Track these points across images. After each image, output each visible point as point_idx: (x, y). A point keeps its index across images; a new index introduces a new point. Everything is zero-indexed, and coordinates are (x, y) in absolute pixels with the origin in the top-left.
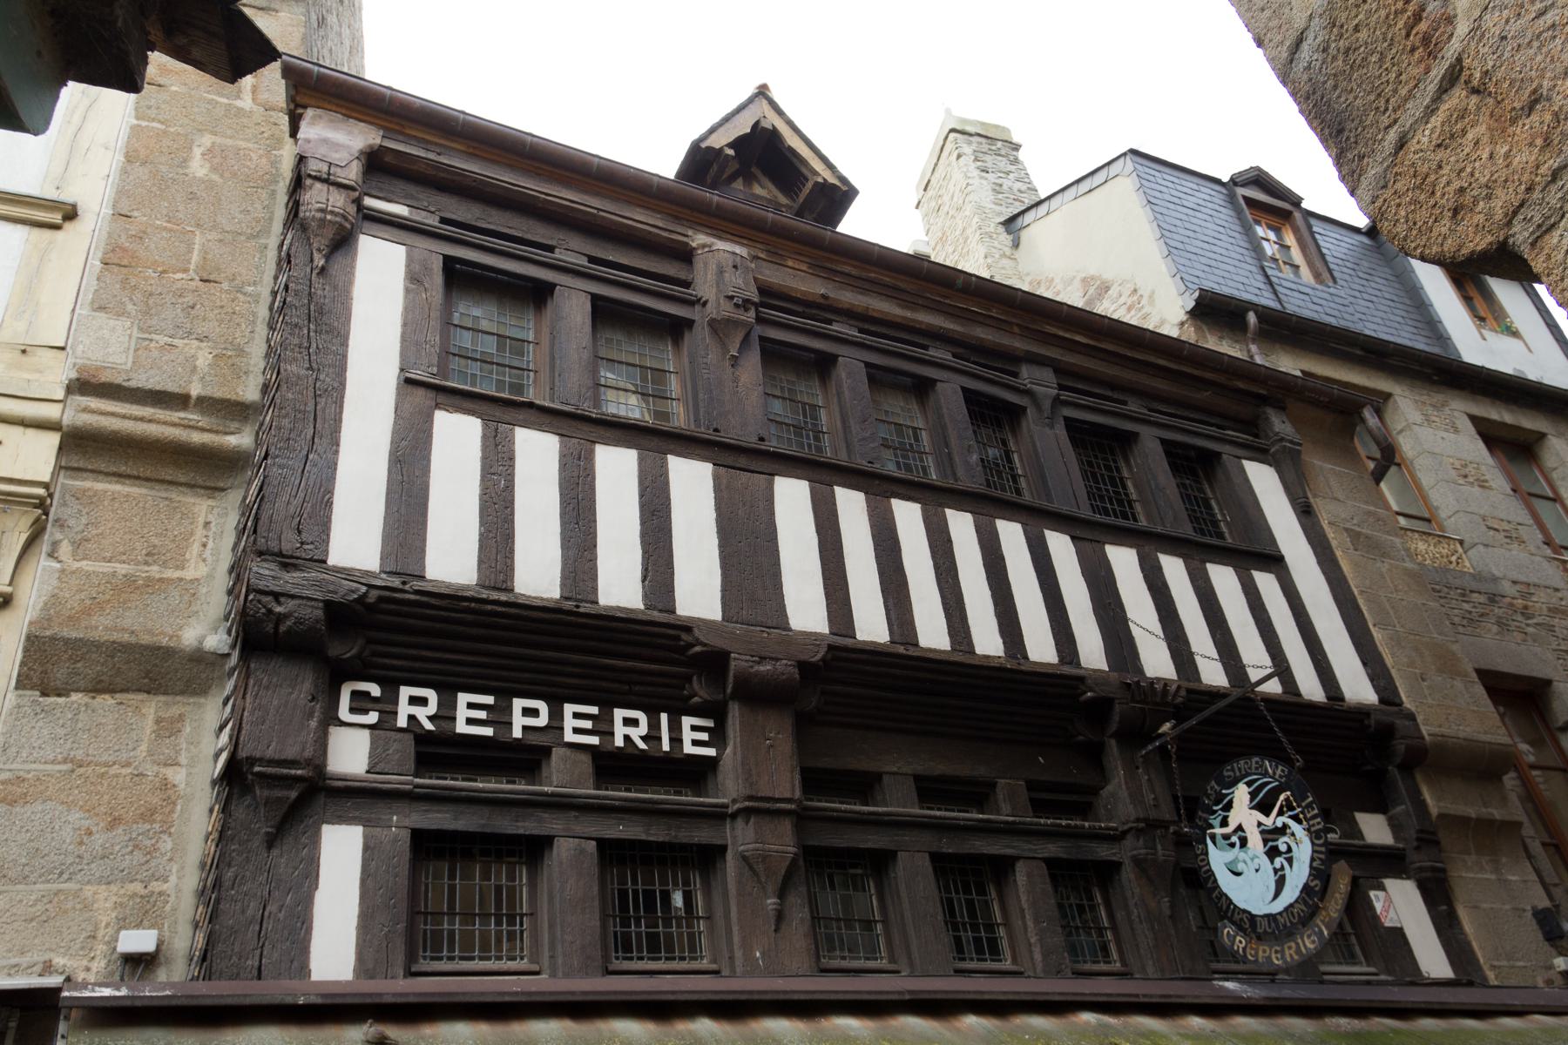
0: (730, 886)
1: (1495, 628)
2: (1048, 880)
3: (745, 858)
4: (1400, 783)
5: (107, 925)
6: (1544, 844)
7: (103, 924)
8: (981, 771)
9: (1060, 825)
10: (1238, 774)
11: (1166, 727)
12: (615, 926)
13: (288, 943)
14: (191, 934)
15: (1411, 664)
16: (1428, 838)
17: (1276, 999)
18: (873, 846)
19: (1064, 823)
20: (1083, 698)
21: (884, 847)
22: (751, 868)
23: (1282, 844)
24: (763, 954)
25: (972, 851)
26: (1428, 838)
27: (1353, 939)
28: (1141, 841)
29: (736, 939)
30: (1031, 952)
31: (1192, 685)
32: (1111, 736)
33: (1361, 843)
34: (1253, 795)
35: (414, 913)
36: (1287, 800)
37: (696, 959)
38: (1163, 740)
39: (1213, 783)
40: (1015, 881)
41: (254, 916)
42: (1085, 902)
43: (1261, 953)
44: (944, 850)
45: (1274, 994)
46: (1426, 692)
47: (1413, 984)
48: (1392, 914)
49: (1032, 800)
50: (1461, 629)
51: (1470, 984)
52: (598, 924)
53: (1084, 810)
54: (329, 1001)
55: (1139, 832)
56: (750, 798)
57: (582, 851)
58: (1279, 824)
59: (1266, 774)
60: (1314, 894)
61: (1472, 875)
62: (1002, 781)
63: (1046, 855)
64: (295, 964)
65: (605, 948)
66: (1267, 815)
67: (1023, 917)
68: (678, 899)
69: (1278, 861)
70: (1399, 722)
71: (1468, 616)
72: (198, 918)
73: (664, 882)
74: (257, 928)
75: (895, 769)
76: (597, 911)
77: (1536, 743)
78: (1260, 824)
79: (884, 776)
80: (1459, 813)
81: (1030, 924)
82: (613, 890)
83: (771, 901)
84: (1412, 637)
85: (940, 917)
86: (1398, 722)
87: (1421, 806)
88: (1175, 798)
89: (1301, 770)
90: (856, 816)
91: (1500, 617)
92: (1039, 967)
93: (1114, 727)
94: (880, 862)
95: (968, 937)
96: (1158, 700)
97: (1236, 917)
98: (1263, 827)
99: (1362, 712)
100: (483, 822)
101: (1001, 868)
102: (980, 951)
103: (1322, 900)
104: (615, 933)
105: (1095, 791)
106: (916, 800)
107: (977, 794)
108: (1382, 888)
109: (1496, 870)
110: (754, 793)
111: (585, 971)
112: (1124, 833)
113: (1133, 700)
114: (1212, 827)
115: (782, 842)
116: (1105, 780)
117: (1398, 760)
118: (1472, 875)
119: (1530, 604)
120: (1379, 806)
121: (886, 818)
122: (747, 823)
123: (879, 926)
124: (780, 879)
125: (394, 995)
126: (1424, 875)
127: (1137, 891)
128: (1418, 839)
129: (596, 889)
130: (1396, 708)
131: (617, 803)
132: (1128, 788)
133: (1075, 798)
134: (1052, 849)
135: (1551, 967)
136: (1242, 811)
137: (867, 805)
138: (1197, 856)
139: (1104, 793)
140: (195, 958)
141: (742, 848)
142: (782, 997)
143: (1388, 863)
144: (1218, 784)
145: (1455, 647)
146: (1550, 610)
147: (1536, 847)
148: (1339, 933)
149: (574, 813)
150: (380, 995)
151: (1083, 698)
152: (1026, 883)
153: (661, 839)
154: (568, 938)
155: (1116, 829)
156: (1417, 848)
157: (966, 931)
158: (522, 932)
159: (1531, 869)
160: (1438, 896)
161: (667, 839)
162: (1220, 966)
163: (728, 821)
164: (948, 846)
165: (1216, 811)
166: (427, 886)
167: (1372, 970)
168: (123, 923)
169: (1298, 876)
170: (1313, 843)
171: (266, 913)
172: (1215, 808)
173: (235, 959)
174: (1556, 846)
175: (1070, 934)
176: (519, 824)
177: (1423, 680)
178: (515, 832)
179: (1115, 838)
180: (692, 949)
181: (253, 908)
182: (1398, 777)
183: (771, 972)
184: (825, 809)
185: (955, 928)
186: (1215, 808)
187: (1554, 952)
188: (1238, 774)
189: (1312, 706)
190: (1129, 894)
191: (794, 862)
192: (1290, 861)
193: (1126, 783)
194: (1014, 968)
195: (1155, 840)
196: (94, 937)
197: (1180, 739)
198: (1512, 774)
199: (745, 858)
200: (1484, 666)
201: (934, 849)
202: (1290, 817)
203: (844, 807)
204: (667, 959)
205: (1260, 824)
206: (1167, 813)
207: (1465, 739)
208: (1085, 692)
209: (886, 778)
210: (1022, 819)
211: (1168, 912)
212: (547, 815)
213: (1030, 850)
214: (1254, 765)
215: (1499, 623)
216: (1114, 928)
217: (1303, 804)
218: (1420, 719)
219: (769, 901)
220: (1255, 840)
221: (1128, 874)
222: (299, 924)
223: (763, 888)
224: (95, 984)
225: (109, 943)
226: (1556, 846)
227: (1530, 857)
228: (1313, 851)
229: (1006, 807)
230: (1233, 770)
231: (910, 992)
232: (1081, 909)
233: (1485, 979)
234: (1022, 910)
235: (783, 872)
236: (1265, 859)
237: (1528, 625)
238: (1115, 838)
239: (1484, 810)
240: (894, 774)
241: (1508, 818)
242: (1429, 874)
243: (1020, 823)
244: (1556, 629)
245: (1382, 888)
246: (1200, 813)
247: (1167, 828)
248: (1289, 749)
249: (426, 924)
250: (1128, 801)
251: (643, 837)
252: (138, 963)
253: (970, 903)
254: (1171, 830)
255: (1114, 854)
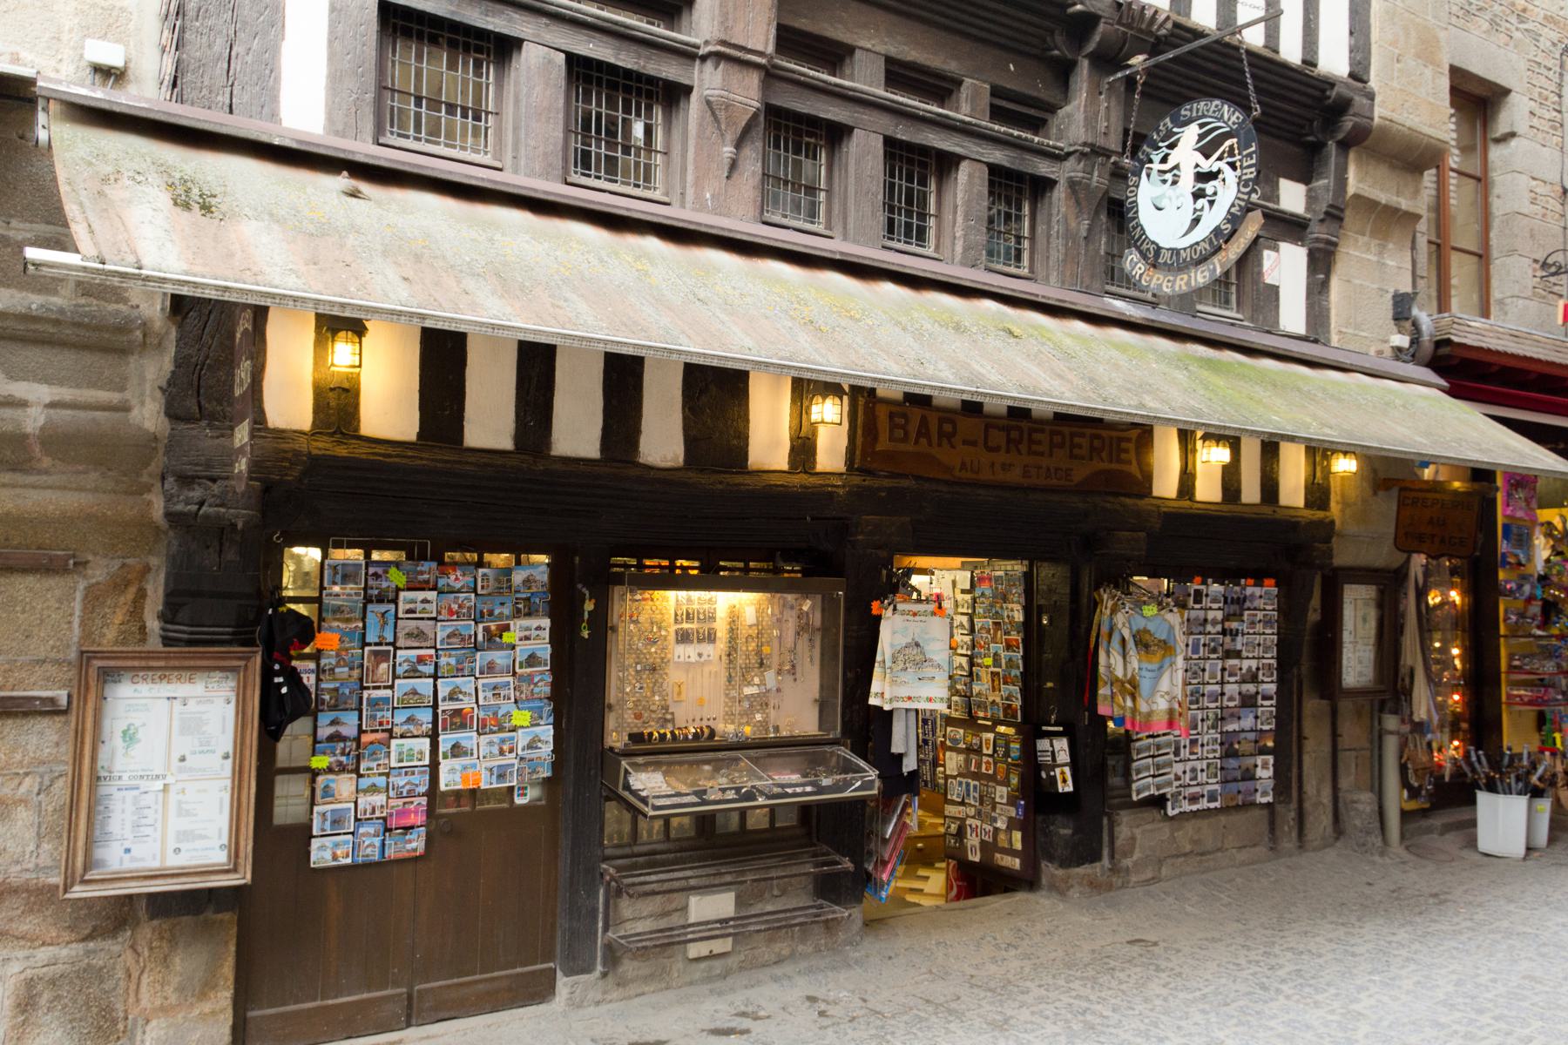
0: (690, 127)
1: (1486, 26)
2: (987, 184)
3: (708, 103)
4: (1333, 159)
5: (71, 30)
6: (1430, 242)
7: (67, 28)
8: (951, 66)
9: (1012, 135)
10: (1194, 114)
11: (1138, 60)
12: (576, 142)
13: (258, 88)
14: (159, 58)
15: (1394, 43)
16: (1334, 215)
17: (1153, 321)
18: (833, 118)
19: (1016, 133)
20: (1071, 10)
21: (845, 122)
22: (713, 114)
23: (1209, 187)
24: (713, 196)
25: (924, 142)
26: (1334, 215)
27: (1234, 289)
28: (1082, 164)
29: (690, 178)
30: (954, 244)
31: (1182, 20)
32: (1085, 57)
33: (1276, 207)
34: (1201, 137)
35: (382, 88)
36: (1231, 147)
37: (649, 189)
38: (1134, 70)
39: (1168, 120)
40: (956, 179)
41: (221, 54)
42: (1013, 211)
43: (1154, 281)
44: (899, 136)
45: (1153, 317)
46: (1396, 74)
47: (1268, 332)
48: (1275, 273)
49: (992, 105)
50: (1454, 20)
51: (1316, 341)
52: (561, 135)
53: (1037, 125)
54: (303, 147)
55: (1083, 155)
56: (724, 43)
57: (550, 62)
58: (1215, 169)
59: (1220, 119)
60: (1221, 238)
61: (1357, 253)
62: (968, 81)
63: (991, 160)
64: (266, 109)
65: (565, 160)
66: (1207, 157)
67: (955, 213)
68: (638, 129)
69: (1202, 202)
70: (1359, 100)
71: (1467, 7)
72: (164, 42)
73: (627, 110)
74: (226, 66)
75: (869, 46)
76: (561, 122)
77: (1466, 150)
78: (1197, 166)
79: (857, 51)
80: (1373, 196)
81: (960, 219)
82: (577, 107)
83: (728, 150)
84: (1407, 15)
85: (881, 197)
86: (1357, 98)
87: (1342, 182)
88: (1126, 132)
89: (1256, 122)
90: (821, 84)
91: (1496, 15)
92: (958, 258)
93: (1091, 47)
94: (836, 134)
95: (900, 221)
96: (1144, 26)
97: (1145, 247)
98: (1199, 169)
99: (1328, 83)
100: (453, 9)
101: (946, 163)
102: (908, 234)
103: (1226, 242)
104: (576, 149)
105: (1052, 109)
106: (883, 82)
107: (940, 87)
108: (1276, 249)
109: (1380, 253)
110: (728, 39)
111: (546, 175)
112: (1069, 154)
113: (1119, 23)
114: (1151, 161)
115: (747, 93)
116: (1066, 99)
117: (1340, 136)
118: (1357, 253)
119: (1530, 7)
120: (1305, 177)
121: (851, 93)
122: (716, 68)
123: (823, 194)
124: (739, 130)
125: (366, 155)
126: (1317, 245)
127: (1063, 210)
128: (1327, 213)
129: (561, 102)
130: (1360, 85)
131: (589, 19)
132: (1085, 111)
133: (1032, 112)
134: (998, 156)
135: (1386, 341)
136: (1186, 153)
137: (834, 76)
138: (1129, 187)
139: (1061, 113)
140: (166, 83)
141: (708, 92)
142: (726, 234)
143: (1286, 227)
144: (1172, 122)
145: (1442, 35)
146: (1546, 17)
147: (1422, 242)
148: (1222, 282)
149: (545, 20)
150: (353, 153)
151: (1071, 10)
152: (967, 184)
153: (629, 66)
154: (533, 143)
155: (1062, 149)
156: (1322, 221)
157: (900, 215)
158: (486, 129)
159: (1409, 258)
160: (1321, 263)
161: (635, 67)
162: (1113, 289)
163: (698, 62)
164: (903, 133)
165: (1161, 148)
166: (393, 62)
167: (1239, 316)
168: (87, 32)
169: (1214, 218)
170: (1239, 191)
171: (233, 53)
172: (1161, 144)
173: (205, 91)
174: (1438, 245)
175: (992, 237)
176: (489, 19)
177: (1398, 61)
178: (484, 26)
179: (1058, 157)
180: (647, 179)
181: (220, 46)
182: (1334, 152)
183: (715, 211)
184: (793, 71)
185: (891, 209)
186: (1161, 144)
187: (1395, 329)
188: (1194, 114)
189: (1285, 66)
190: (1055, 211)
191: (755, 116)
192: (1211, 203)
193: (1086, 106)
194: (936, 255)
195: (1093, 167)
196: (59, 39)
197: (1149, 72)
198: (1433, 171)
199: (708, 103)
200: (1457, 63)
201: (889, 133)
202: (1228, 163)
203: (812, 73)
204: (623, 183)
205: (1197, 166)
206: (1114, 143)
207: (1409, 129)
208: (1075, 4)
209: (858, 54)
210: (978, 122)
211: (1085, 234)
212: (517, 16)
213: (978, 152)
214: (1213, 108)
215: (1492, 22)
216: (1032, 239)
217: (1245, 153)
218: (1378, 100)
219: (725, 149)
220: (1187, 182)
221: (1059, 194)
222: (267, 72)
223: (722, 135)
224: (70, 82)
225: (75, 48)
226: (1438, 245)
227: (1413, 248)
228: (1237, 198)
229: (965, 107)
230: (1191, 110)
231: (842, 253)
232: (1008, 217)
233: (1329, 340)
234: (956, 207)
235: (743, 123)
236: (1191, 198)
237: (1517, 29)
238: (1058, 157)
239: (1395, 198)
240: (868, 50)
241: (1411, 210)
242: (1321, 245)
243: (975, 125)
244: (1542, 39)
245: (1276, 249)
246: (1145, 147)
247: (1109, 157)
248: (1253, 96)
249: (393, 101)
250: (1082, 123)
251: (612, 60)
252: (105, 73)
253: (910, 192)
254: (1113, 159)
255: (1053, 172)
